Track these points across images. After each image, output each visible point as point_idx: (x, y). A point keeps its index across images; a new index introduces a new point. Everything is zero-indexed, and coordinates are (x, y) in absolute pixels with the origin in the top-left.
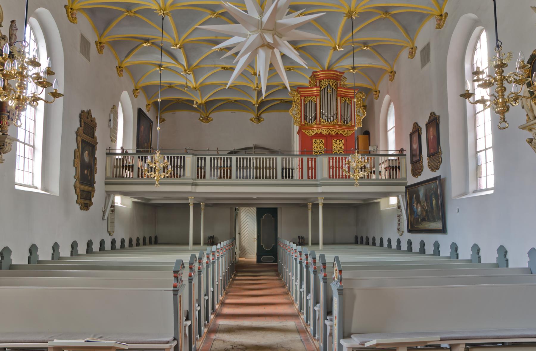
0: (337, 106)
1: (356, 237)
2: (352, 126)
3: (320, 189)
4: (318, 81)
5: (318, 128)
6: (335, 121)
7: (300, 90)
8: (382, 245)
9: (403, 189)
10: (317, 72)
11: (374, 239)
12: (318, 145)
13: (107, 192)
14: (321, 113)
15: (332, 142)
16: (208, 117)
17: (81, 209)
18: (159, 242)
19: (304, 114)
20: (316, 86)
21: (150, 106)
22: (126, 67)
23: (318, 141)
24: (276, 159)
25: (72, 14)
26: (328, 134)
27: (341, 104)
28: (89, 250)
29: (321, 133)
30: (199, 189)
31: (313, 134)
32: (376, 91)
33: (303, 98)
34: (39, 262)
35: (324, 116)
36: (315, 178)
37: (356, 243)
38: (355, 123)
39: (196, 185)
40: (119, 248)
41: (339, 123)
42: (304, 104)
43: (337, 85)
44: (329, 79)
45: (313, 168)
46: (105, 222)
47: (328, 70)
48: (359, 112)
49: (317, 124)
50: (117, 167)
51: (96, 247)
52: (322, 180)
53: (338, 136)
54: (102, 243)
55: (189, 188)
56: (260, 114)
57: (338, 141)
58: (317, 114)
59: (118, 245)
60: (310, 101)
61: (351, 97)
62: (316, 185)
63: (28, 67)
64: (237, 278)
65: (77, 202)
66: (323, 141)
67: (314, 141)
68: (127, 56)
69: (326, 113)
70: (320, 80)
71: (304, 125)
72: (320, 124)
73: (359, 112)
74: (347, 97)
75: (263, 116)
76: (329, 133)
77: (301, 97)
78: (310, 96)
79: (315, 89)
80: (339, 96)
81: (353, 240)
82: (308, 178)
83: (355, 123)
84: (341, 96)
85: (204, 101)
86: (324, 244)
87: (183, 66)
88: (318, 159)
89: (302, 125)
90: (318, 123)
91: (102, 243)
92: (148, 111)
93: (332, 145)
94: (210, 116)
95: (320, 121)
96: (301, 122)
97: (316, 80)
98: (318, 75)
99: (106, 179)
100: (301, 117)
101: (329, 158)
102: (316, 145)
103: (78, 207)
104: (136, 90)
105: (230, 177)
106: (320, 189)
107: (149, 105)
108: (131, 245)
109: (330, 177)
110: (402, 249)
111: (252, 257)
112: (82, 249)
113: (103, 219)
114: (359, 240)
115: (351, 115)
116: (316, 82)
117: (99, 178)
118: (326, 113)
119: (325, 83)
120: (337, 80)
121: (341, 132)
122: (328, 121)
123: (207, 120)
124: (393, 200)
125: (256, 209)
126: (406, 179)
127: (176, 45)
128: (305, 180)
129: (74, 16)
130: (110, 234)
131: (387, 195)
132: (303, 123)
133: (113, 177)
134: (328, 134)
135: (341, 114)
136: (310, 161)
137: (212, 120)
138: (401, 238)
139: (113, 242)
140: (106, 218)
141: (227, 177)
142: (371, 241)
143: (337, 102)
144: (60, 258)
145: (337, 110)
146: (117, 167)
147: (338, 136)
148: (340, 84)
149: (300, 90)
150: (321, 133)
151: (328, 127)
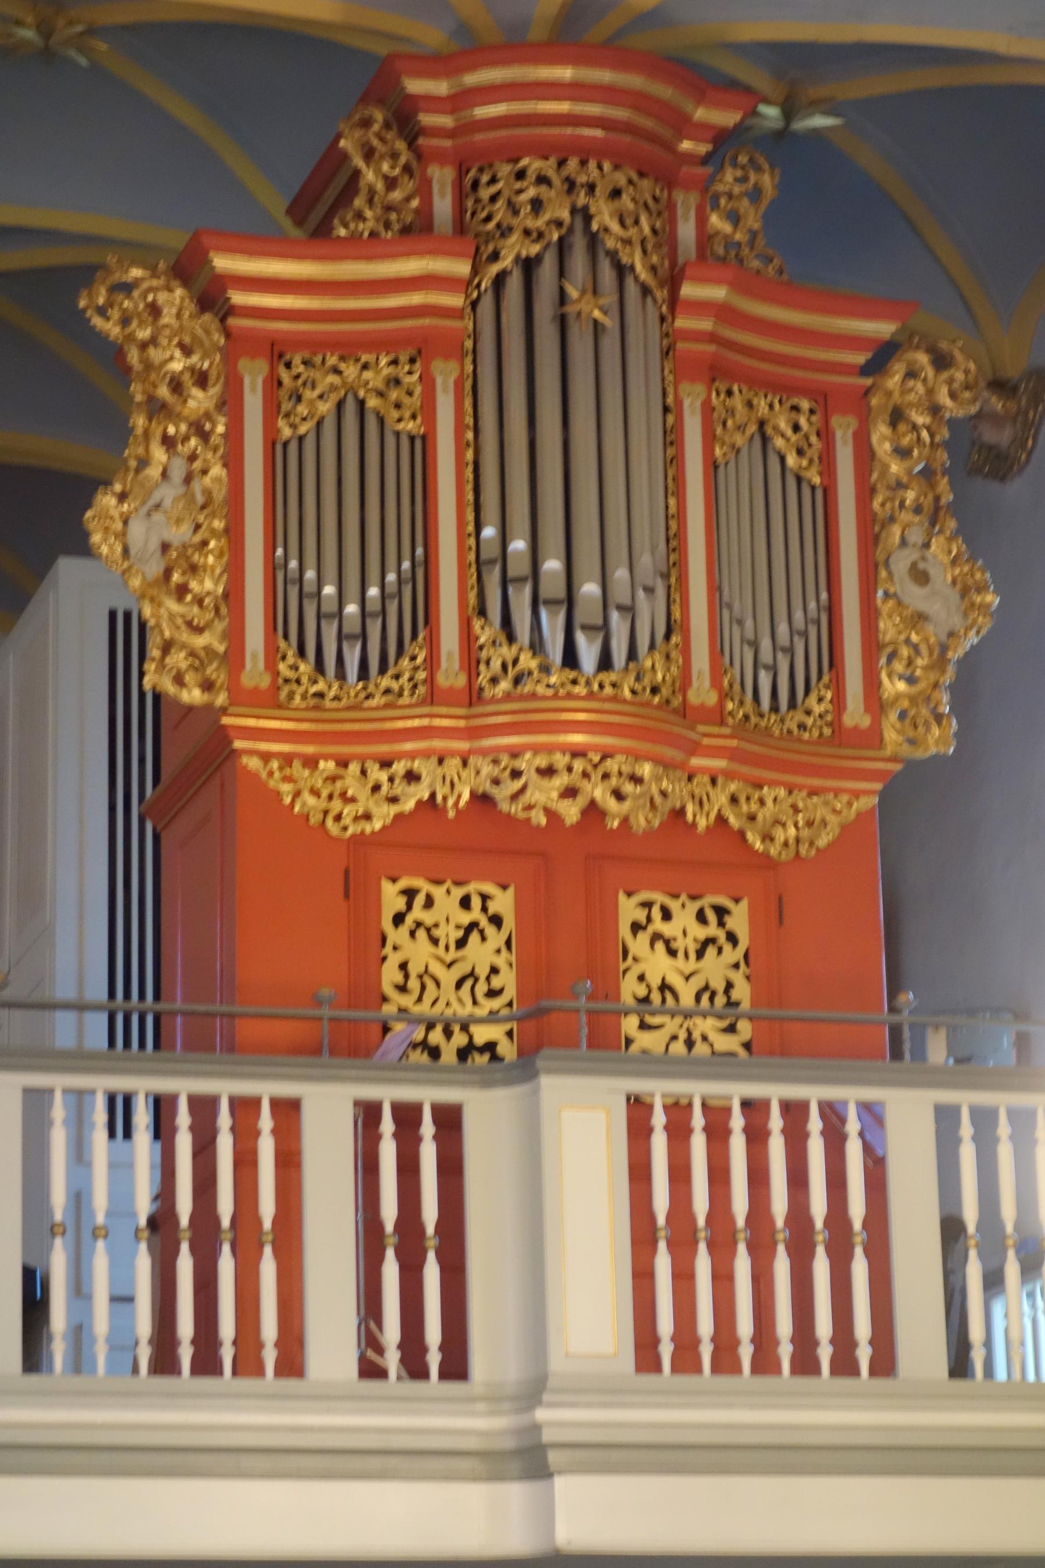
2: (839, 734)
14: (477, 564)
20: (417, 231)
24: (288, 1111)
27: (712, 467)
31: (383, 815)
35: (521, 600)
43: (665, 238)
44: (586, 153)
45: (419, 1246)
48: (921, 577)
66: (503, 902)
72: (473, 696)
73: (921, 577)
76: (593, 811)
78: (348, 348)
84: (715, 373)
90: (451, 674)
95: (471, 660)
96: (234, 656)
116: (425, 190)
122: (570, 658)
128: (329, 1397)
132: (254, 673)
134: (571, 812)
143: (673, 438)
145: (675, 542)
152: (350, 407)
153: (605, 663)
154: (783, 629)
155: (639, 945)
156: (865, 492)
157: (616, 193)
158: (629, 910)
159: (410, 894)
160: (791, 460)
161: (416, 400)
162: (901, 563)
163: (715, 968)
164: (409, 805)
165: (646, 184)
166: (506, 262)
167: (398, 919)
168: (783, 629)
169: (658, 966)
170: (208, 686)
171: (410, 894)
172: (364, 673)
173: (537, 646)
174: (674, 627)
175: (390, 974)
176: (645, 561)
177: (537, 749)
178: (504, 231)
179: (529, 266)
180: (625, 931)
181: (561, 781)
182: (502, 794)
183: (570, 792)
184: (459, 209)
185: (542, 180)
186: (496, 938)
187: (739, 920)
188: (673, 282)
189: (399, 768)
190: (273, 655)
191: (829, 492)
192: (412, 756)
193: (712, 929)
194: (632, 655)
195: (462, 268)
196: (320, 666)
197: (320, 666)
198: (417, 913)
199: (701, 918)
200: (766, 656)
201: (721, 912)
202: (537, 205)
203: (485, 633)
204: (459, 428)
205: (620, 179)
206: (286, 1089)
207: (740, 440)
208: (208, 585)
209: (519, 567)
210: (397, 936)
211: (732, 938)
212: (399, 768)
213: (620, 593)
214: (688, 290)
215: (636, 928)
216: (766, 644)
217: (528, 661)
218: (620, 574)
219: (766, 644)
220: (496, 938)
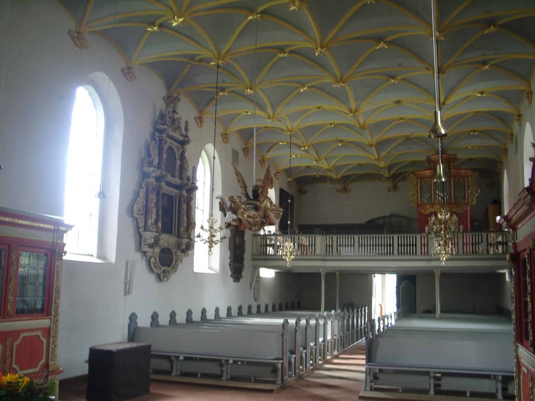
0: (450, 185)
2: (465, 203)
4: (432, 164)
13: (253, 266)
16: (346, 188)
17: (234, 281)
20: (430, 169)
22: (269, 159)
25: (226, 138)
27: (454, 184)
28: (240, 314)
33: (419, 180)
34: (208, 320)
38: (468, 200)
39: (325, 260)
40: (264, 312)
46: (252, 291)
50: (261, 246)
51: (245, 311)
54: (250, 308)
59: (263, 309)
62: (428, 260)
63: (156, 26)
65: (231, 276)
68: (268, 151)
75: (399, 184)
83: (468, 200)
85: (339, 177)
86: (442, 311)
90: (433, 202)
91: (250, 308)
96: (418, 201)
99: (253, 255)
100: (417, 197)
103: (232, 280)
104: (278, 173)
108: (274, 310)
112: (235, 312)
113: (251, 288)
117: (247, 256)
121: (454, 210)
127: (305, 147)
129: (227, 139)
130: (256, 300)
132: (419, 203)
135: (454, 192)
139: (259, 307)
140: (253, 287)
144: (219, 318)
146: (261, 246)
148: (453, 166)
191: (465, 184)
208: (416, 196)
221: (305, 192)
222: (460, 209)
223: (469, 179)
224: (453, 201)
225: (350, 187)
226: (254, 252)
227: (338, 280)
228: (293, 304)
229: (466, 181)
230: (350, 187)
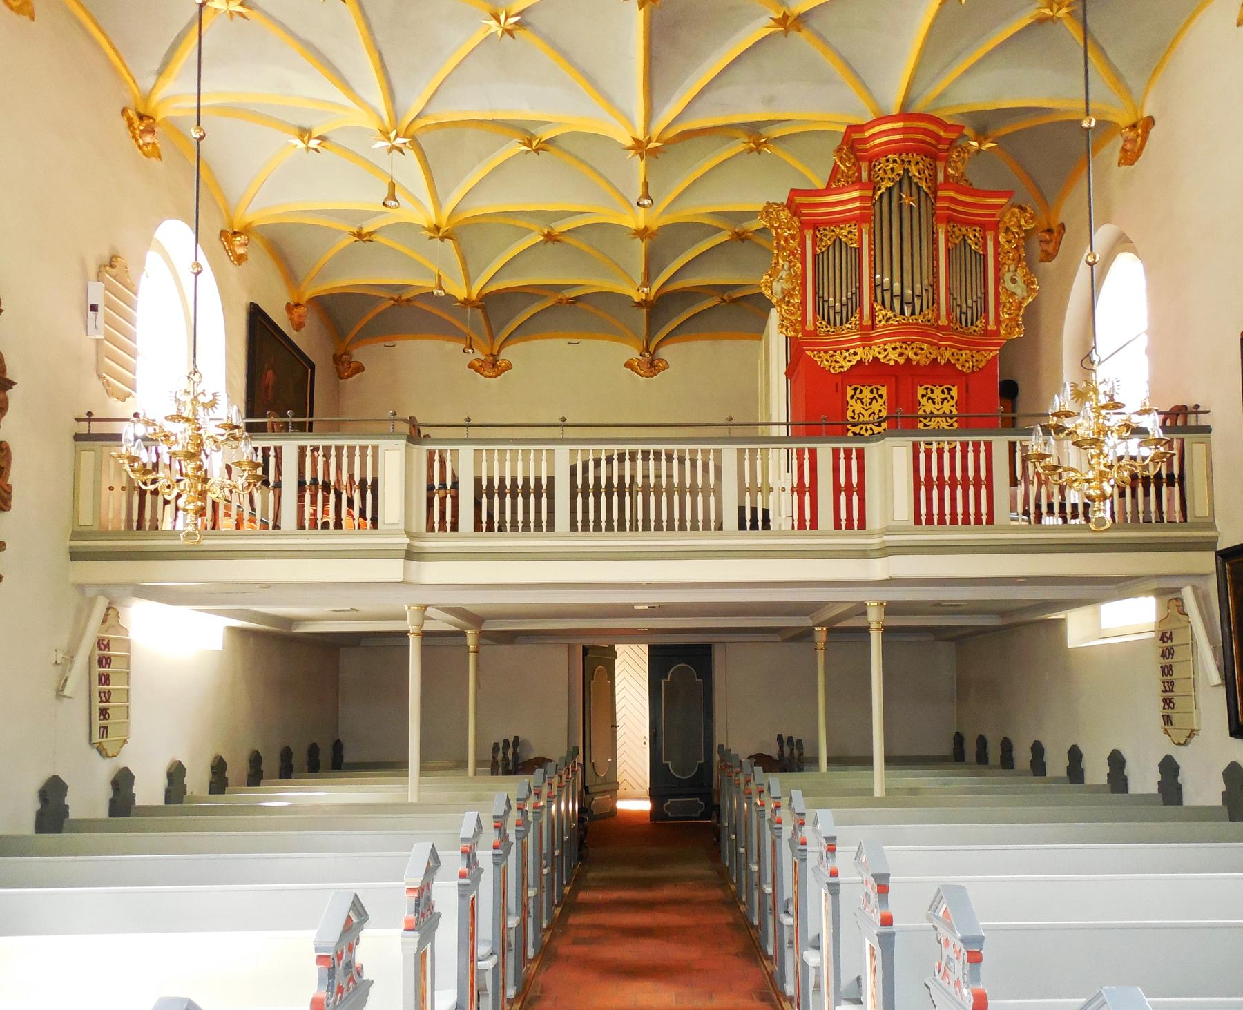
0: (936, 257)
1: (959, 739)
2: (986, 332)
3: (878, 569)
5: (866, 341)
6: (929, 314)
7: (799, 200)
8: (1038, 766)
9: (1206, 562)
10: (860, 128)
11: (1007, 746)
12: (865, 404)
14: (874, 287)
15: (915, 393)
16: (495, 357)
18: (347, 758)
19: (815, 293)
21: (301, 310)
23: (866, 394)
26: (901, 361)
27: (948, 250)
29: (876, 359)
30: (432, 572)
31: (847, 365)
32: (1050, 231)
33: (809, 234)
35: (887, 296)
36: (862, 525)
37: (958, 756)
41: (943, 322)
42: (815, 256)
43: (934, 177)
44: (908, 151)
45: (852, 490)
47: (904, 115)
48: (1014, 281)
49: (862, 328)
52: (887, 531)
53: (937, 373)
55: (393, 569)
56: (656, 349)
57: (938, 390)
58: (860, 288)
60: (837, 242)
61: (984, 227)
62: (864, 553)
64: (583, 896)
66: (883, 391)
67: (850, 392)
69: (897, 285)
70: (872, 160)
71: (814, 333)
72: (873, 327)
73: (1014, 281)
74: (971, 224)
75: (666, 352)
76: (908, 360)
77: (802, 230)
78: (837, 223)
79: (856, 194)
80: (940, 219)
81: (946, 749)
82: (837, 526)
84: (949, 220)
86: (831, 761)
87: (374, 111)
88: (873, 452)
89: (805, 332)
90: (867, 321)
92: (298, 326)
93: (915, 404)
94: (502, 356)
97: (858, 159)
98: (866, 141)
101: (916, 446)
102: (858, 407)
104: (297, 305)
105: (814, 526)
106: (878, 569)
107: (297, 305)
109: (917, 521)
110: (1187, 801)
111: (635, 802)
114: (971, 749)
115: (986, 294)
118: (897, 285)
119: (889, 170)
120: (935, 158)
121: (948, 355)
122: (902, 313)
123: (494, 365)
124: (1131, 618)
125: (645, 648)
126: (1211, 526)
128: (826, 535)
131: (1120, 586)
132: (810, 326)
133: (129, 527)
134: (901, 361)
135: (948, 289)
136: (842, 463)
137: (509, 367)
138: (1182, 757)
141: (538, 527)
142: (994, 752)
143: (935, 242)
145: (936, 275)
147: (937, 373)
148: (947, 176)
149: (799, 200)
150: (876, 359)
151: (908, 334)
152: (837, 243)
153: (913, 313)
154: (969, 301)
155: (924, 401)
156: (996, 254)
157: (917, 163)
158: (921, 391)
159: (855, 389)
160: (973, 247)
161: (856, 238)
162: (1007, 277)
163: (947, 407)
164: (854, 363)
165: (928, 160)
166: (883, 190)
167: (852, 397)
168: (969, 301)
169: (929, 407)
170: (795, 331)
171: (855, 389)
172: (841, 324)
173: (892, 309)
174: (936, 301)
175: (849, 414)
176: (925, 282)
177: (891, 342)
178: (882, 180)
179: (889, 190)
180: (919, 397)
181: (900, 350)
182: (881, 357)
183: (901, 355)
184: (870, 175)
185: (895, 161)
186: (952, 402)
187: (954, 392)
188: (935, 192)
189: (852, 351)
190: (815, 320)
191: (985, 256)
192: (855, 347)
193: (946, 395)
194: (921, 310)
195: (870, 193)
196: (829, 322)
197: (829, 322)
198: (858, 395)
199: (943, 392)
200: (964, 309)
201: (949, 390)
202: (892, 169)
203: (877, 307)
204: (870, 244)
205: (919, 158)
206: (278, 443)
207: (957, 241)
208: (797, 300)
209: (886, 286)
210: (852, 402)
211: (952, 398)
212: (852, 351)
213: (917, 292)
214: (940, 193)
215: (923, 396)
216: (964, 306)
217: (890, 314)
218: (918, 286)
219: (964, 306)
220: (881, 401)
221: (360, 369)
222: (965, 354)
223: (1002, 239)
224: (943, 322)
225: (508, 354)
226: (86, 519)
227: (472, 657)
228: (313, 751)
229: (990, 244)
230: (508, 354)
